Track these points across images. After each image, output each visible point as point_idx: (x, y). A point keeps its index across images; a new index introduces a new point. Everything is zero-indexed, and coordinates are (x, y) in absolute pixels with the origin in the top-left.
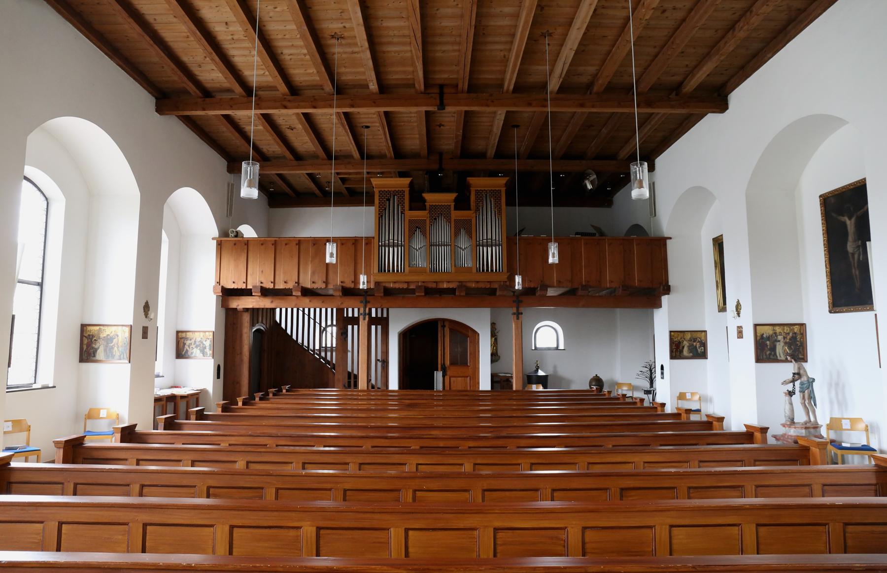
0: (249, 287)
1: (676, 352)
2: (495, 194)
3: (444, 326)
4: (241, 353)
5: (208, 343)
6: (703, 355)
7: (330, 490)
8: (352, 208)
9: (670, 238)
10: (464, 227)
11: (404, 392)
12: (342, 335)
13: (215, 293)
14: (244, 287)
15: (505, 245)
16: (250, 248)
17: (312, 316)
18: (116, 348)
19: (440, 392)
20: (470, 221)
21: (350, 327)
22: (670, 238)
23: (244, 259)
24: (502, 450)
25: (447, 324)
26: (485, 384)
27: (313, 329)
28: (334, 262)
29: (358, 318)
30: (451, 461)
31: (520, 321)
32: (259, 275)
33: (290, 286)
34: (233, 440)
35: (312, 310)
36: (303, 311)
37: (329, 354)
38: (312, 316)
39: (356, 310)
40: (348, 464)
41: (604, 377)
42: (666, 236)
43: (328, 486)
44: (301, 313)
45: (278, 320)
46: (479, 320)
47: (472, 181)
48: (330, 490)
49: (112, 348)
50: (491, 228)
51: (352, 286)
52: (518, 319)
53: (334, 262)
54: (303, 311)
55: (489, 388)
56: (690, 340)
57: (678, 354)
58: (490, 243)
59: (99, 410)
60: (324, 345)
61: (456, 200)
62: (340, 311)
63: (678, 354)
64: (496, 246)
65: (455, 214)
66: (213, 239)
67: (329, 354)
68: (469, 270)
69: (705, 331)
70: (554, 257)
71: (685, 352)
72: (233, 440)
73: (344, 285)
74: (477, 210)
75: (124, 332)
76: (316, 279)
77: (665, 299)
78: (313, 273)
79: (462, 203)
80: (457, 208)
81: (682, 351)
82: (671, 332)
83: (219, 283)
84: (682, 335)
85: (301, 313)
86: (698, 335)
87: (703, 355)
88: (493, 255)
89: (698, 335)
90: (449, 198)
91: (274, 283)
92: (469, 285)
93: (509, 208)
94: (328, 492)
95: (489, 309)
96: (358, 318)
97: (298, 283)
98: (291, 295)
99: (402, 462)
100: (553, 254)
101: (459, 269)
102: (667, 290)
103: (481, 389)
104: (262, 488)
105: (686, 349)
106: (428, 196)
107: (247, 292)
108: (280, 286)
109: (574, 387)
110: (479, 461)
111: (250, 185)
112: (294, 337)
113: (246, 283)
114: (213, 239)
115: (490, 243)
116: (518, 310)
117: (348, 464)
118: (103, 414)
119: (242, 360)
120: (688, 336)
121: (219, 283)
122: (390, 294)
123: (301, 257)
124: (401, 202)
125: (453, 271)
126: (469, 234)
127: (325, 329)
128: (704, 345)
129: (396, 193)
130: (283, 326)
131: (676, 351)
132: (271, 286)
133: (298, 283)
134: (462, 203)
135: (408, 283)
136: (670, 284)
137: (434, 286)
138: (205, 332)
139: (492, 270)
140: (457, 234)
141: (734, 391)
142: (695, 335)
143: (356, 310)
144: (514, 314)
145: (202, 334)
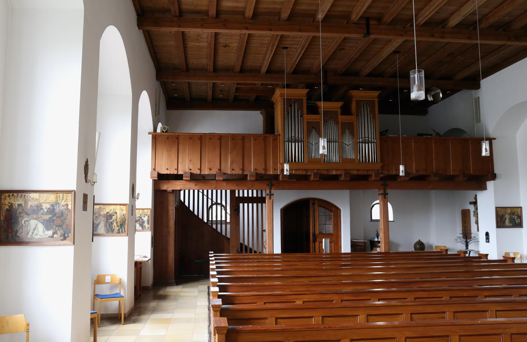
0: (179, 173)
1: (500, 223)
2: (370, 103)
3: (314, 204)
4: (168, 226)
5: (145, 219)
6: (520, 225)
7: (499, 334)
8: (232, 111)
9: (495, 139)
10: (349, 128)
11: (286, 255)
12: (235, 211)
13: (151, 177)
14: (175, 173)
15: (378, 143)
16: (180, 141)
17: (210, 196)
18: (115, 224)
19: (328, 254)
20: (353, 123)
21: (241, 205)
22: (495, 139)
23: (218, 152)
24: (406, 300)
25: (316, 202)
26: (346, 247)
27: (211, 206)
28: (326, 153)
29: (265, 198)
30: (521, 308)
31: (271, 200)
32: (187, 164)
33: (214, 172)
34: (306, 298)
35: (210, 191)
36: (203, 193)
37: (219, 226)
38: (210, 196)
39: (255, 191)
40: (444, 312)
41: (424, 241)
42: (492, 137)
43: (499, 331)
44: (201, 194)
45: (183, 200)
46: (342, 200)
47: (354, 93)
48: (499, 334)
49: (112, 223)
50: (368, 129)
51: (263, 172)
52: (385, 198)
53: (326, 153)
54: (203, 193)
55: (349, 251)
56: (510, 214)
57: (502, 224)
58: (290, 140)
59: (104, 276)
60: (210, 219)
61: (341, 107)
62: (233, 193)
63: (502, 224)
64: (371, 143)
65: (342, 118)
66: (149, 133)
67: (219, 226)
68: (352, 161)
69: (521, 208)
70: (486, 151)
71: (507, 223)
72: (306, 298)
73: (257, 171)
74: (357, 116)
75: (122, 210)
76: (234, 167)
77: (490, 184)
78: (232, 163)
79: (346, 110)
80: (343, 114)
81: (504, 222)
82: (496, 208)
83: (154, 169)
84: (504, 210)
85: (201, 194)
86: (516, 210)
87: (520, 225)
88: (369, 151)
89: (516, 210)
90: (336, 106)
91: (200, 169)
92: (352, 172)
93: (381, 115)
94: (498, 336)
95: (348, 191)
96: (265, 198)
97: (220, 170)
98: (182, 179)
99: (484, 309)
100: (486, 149)
101: (345, 161)
102: (493, 177)
103: (343, 251)
104: (448, 336)
105: (507, 220)
106: (322, 105)
107: (178, 177)
108: (206, 172)
109: (401, 250)
110: (499, 309)
111: (419, 90)
112: (196, 213)
113: (177, 169)
114: (149, 133)
115: (290, 140)
116: (385, 191)
117: (444, 312)
118: (108, 279)
119: (169, 232)
120: (509, 211)
121: (154, 169)
122: (272, 181)
123: (222, 149)
124: (300, 108)
125: (341, 161)
126: (353, 134)
127: (211, 207)
128: (520, 217)
129: (296, 101)
130: (187, 204)
131: (501, 222)
132: (198, 172)
133: (220, 170)
134: (346, 110)
135: (306, 170)
136: (495, 172)
137: (326, 173)
138: (143, 209)
139: (295, 161)
140: (343, 133)
141: (492, 251)
142: (514, 210)
143: (255, 191)
144: (382, 194)
145: (141, 211)
